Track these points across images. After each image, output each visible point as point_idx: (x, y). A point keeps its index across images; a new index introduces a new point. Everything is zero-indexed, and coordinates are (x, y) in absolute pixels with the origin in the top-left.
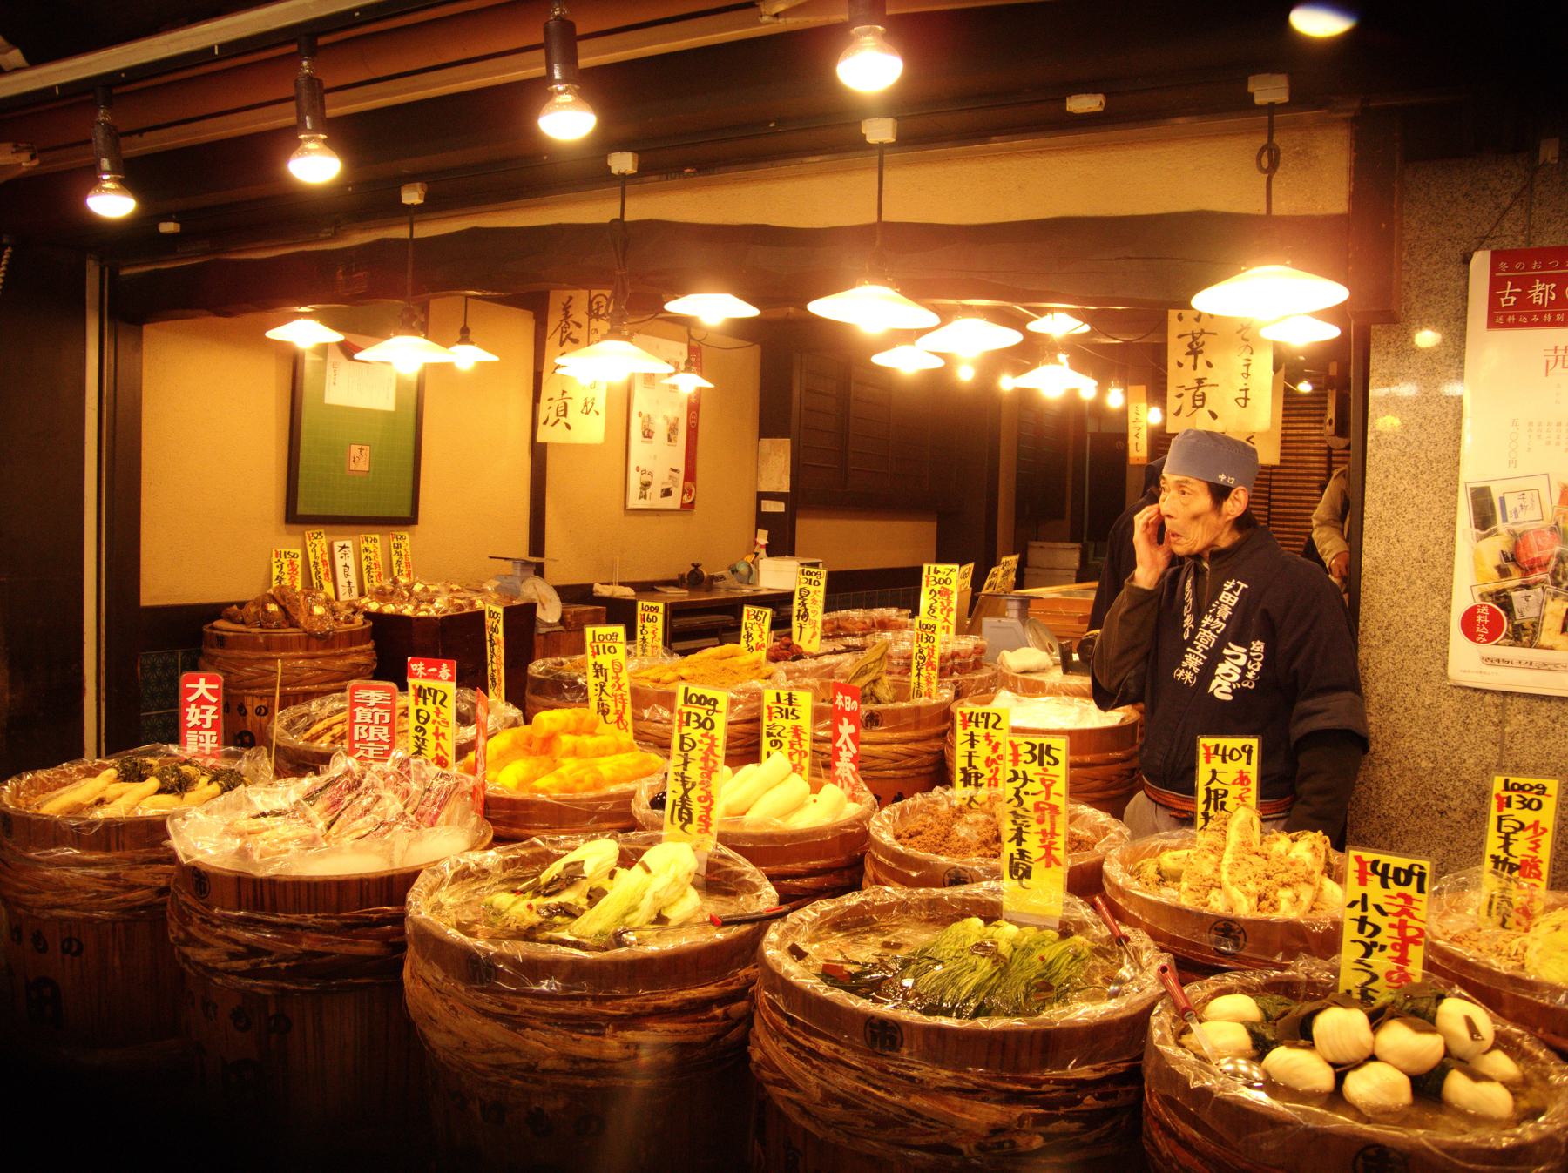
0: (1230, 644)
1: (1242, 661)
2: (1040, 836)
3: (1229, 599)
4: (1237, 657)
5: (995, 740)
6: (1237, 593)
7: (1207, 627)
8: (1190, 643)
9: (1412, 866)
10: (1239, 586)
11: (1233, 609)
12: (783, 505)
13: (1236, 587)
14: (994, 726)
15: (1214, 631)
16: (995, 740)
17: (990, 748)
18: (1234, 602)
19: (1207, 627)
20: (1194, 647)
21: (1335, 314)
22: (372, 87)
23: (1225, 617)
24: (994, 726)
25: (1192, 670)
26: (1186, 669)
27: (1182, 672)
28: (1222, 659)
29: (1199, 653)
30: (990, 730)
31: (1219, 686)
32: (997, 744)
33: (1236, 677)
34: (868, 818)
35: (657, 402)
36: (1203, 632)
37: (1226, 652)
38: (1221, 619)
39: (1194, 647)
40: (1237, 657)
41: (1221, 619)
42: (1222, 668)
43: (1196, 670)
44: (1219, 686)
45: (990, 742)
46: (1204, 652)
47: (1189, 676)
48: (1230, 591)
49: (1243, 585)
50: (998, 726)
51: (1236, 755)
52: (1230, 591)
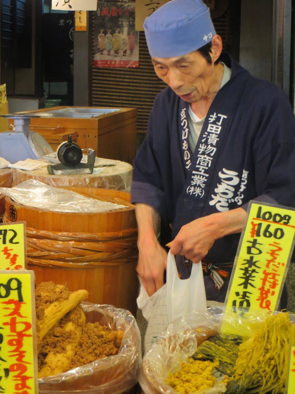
0: (224, 170)
1: (236, 181)
2: (243, 272)
3: (214, 129)
4: (230, 179)
5: (12, 253)
6: (220, 124)
7: (203, 153)
8: (194, 167)
9: (10, 281)
10: (220, 117)
11: (219, 136)
13: (218, 119)
14: (11, 241)
15: (209, 155)
16: (12, 253)
17: (9, 261)
18: (219, 130)
19: (203, 153)
20: (198, 170)
21: (217, 187)
23: (214, 143)
24: (11, 241)
25: (199, 186)
26: (195, 186)
27: (192, 189)
28: (219, 181)
29: (202, 173)
30: (8, 245)
31: (219, 202)
32: (15, 256)
33: (231, 195)
34: (222, 284)
35: (81, 28)
36: (201, 158)
37: (221, 175)
38: (212, 145)
39: (198, 170)
40: (230, 179)
41: (212, 145)
42: (221, 188)
43: (203, 186)
44: (219, 202)
45: (9, 255)
46: (206, 172)
47: (198, 191)
48: (214, 123)
49: (223, 117)
50: (14, 241)
51: (267, 216)
52: (214, 123)
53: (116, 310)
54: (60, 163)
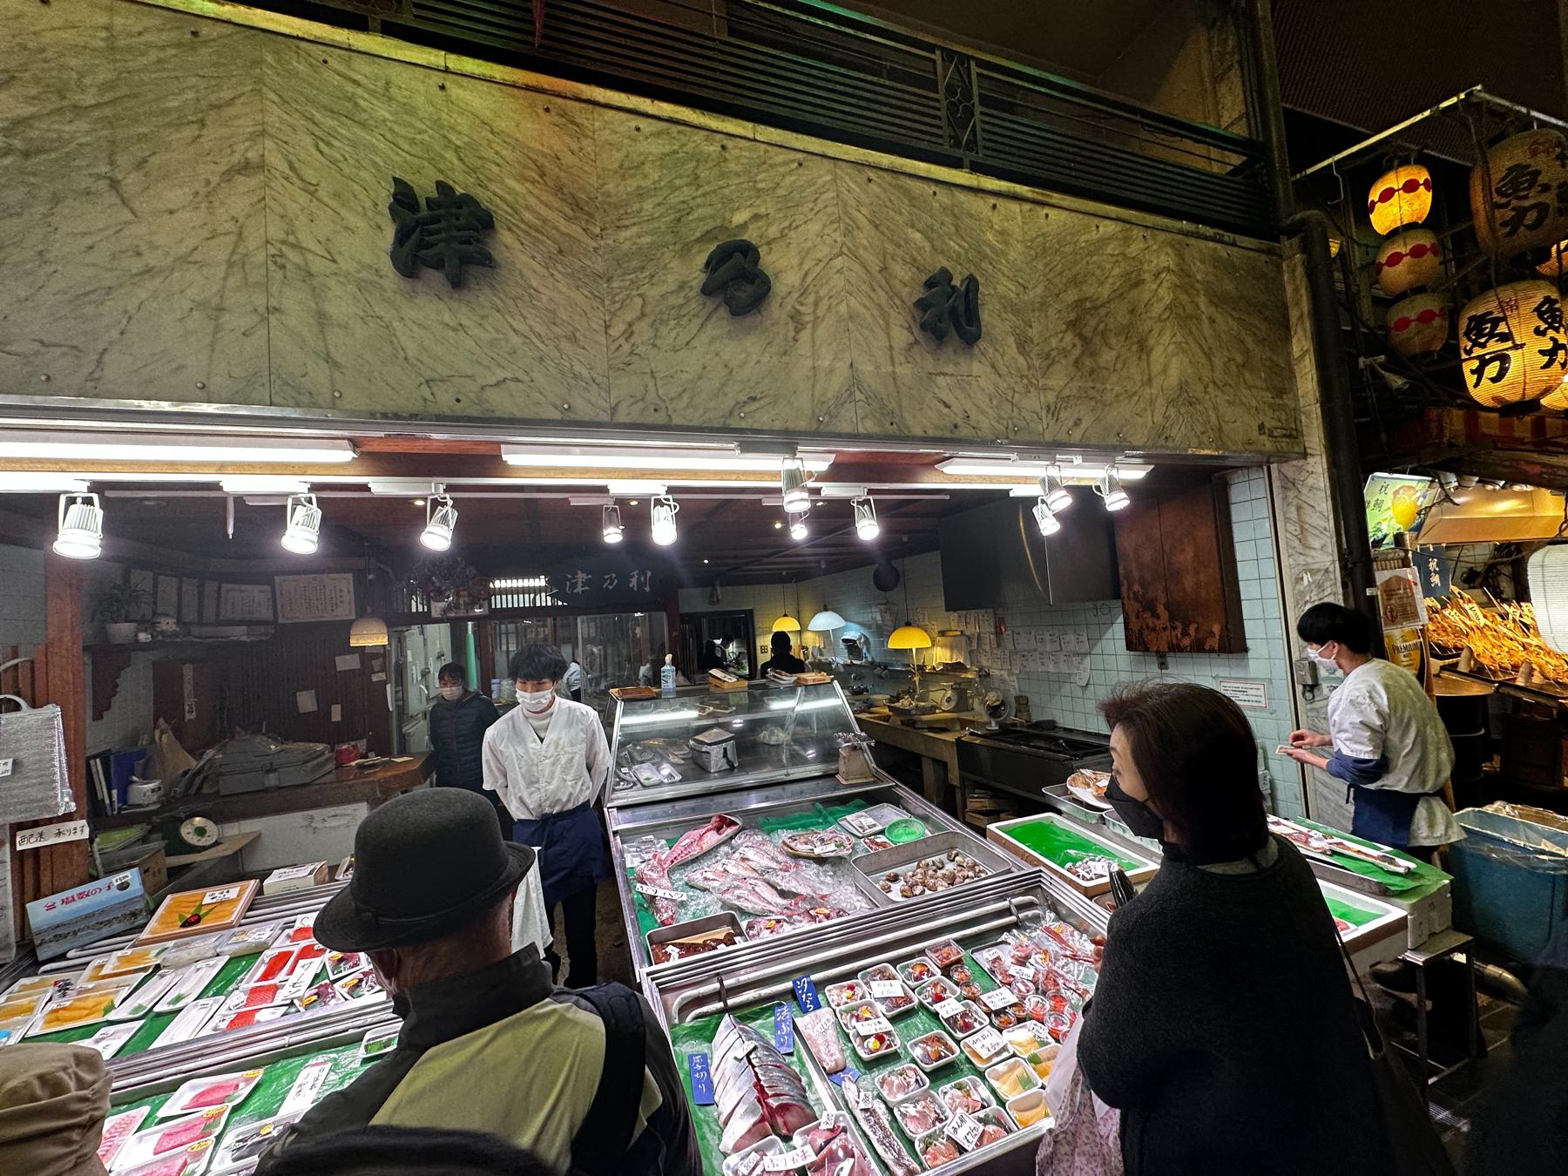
12: (334, 707)
22: (71, 434)
53: (259, 981)
54: (1245, 158)
